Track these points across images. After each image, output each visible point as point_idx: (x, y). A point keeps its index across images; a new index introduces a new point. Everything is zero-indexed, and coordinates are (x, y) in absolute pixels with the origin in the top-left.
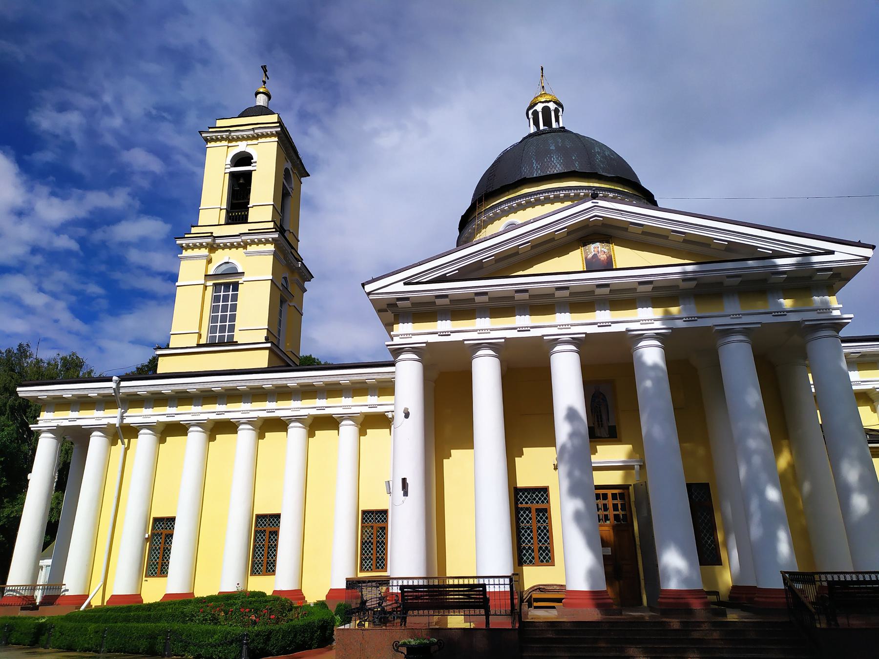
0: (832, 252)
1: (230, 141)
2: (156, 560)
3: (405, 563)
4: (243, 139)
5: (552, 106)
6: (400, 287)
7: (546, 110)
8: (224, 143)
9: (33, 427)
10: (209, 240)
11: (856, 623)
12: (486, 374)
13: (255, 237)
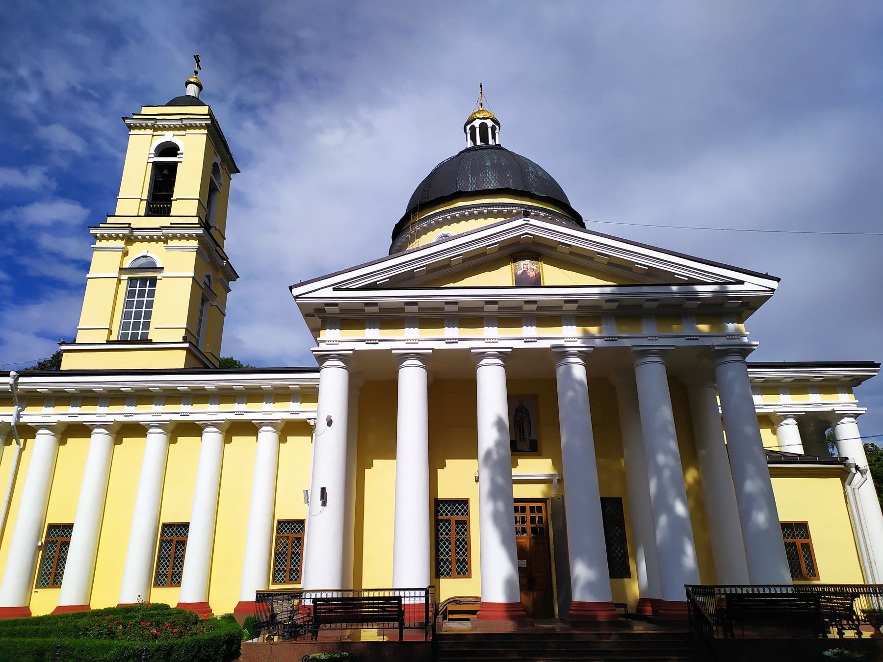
0: (742, 283)
1: (155, 130)
4: (170, 128)
5: (489, 123)
6: (329, 293)
8: (151, 132)
10: (126, 232)
12: (412, 385)
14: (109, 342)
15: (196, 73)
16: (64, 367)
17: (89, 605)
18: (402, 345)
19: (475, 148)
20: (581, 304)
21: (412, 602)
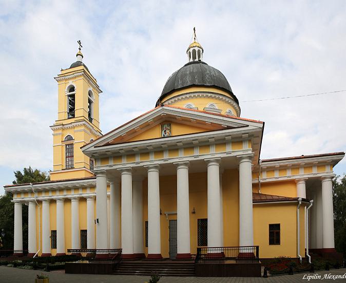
0: (248, 126)
1: (66, 80)
2: (54, 245)
3: (215, 241)
4: (70, 79)
5: (197, 49)
6: (93, 149)
7: (194, 51)
8: (64, 82)
9: (12, 201)
10: (61, 126)
11: (309, 277)
12: (153, 180)
13: (78, 123)
14: (63, 170)
15: (80, 49)
16: (51, 180)
17: (120, 250)
18: (177, 160)
19: (194, 63)
20: (154, 146)
21: (217, 252)
